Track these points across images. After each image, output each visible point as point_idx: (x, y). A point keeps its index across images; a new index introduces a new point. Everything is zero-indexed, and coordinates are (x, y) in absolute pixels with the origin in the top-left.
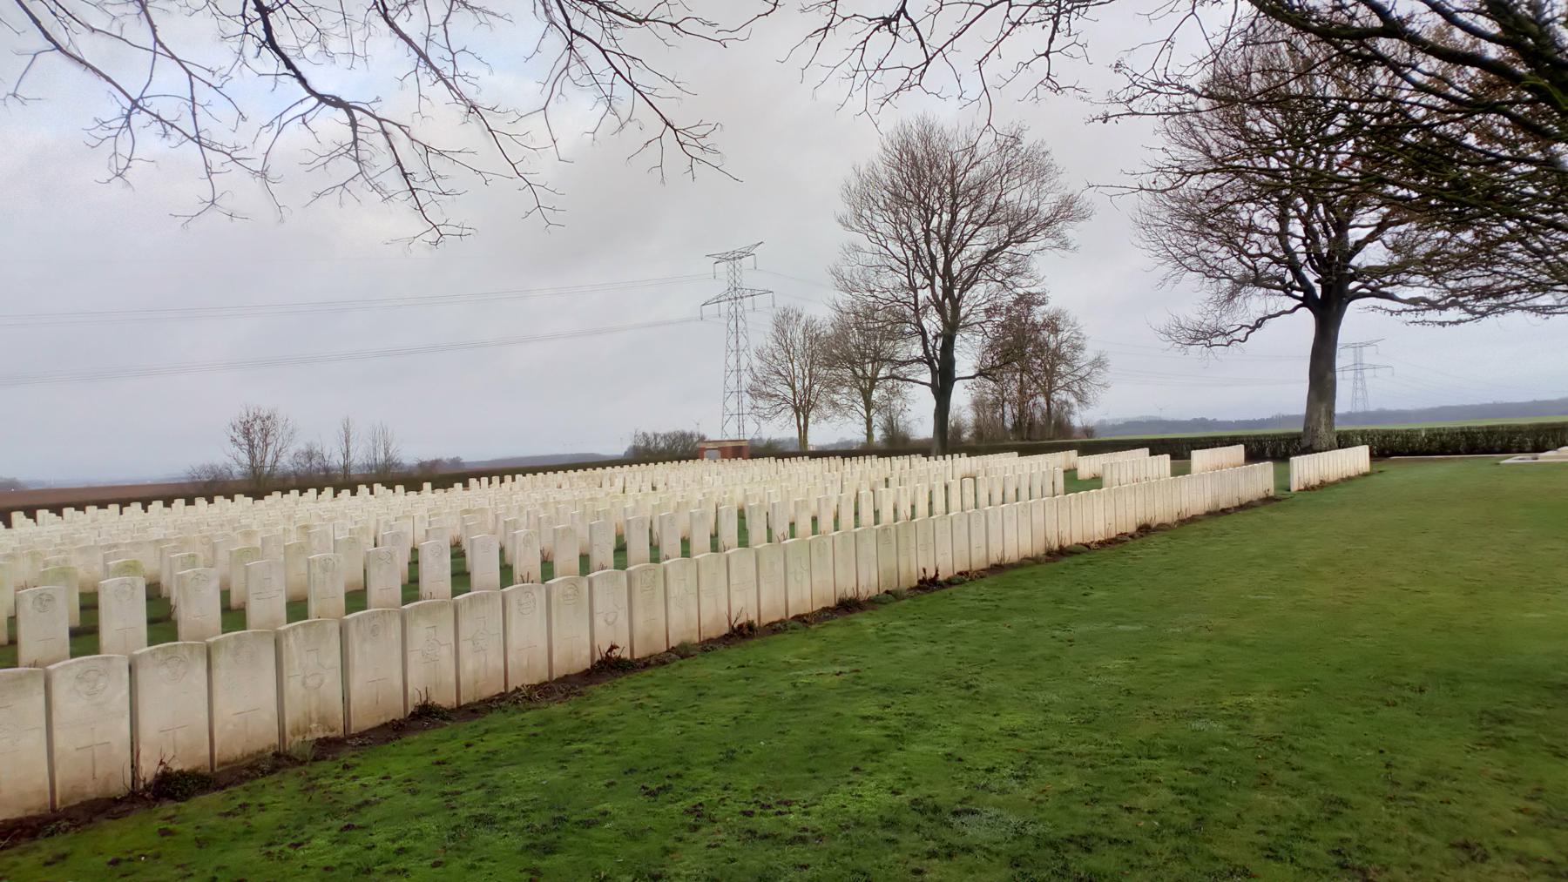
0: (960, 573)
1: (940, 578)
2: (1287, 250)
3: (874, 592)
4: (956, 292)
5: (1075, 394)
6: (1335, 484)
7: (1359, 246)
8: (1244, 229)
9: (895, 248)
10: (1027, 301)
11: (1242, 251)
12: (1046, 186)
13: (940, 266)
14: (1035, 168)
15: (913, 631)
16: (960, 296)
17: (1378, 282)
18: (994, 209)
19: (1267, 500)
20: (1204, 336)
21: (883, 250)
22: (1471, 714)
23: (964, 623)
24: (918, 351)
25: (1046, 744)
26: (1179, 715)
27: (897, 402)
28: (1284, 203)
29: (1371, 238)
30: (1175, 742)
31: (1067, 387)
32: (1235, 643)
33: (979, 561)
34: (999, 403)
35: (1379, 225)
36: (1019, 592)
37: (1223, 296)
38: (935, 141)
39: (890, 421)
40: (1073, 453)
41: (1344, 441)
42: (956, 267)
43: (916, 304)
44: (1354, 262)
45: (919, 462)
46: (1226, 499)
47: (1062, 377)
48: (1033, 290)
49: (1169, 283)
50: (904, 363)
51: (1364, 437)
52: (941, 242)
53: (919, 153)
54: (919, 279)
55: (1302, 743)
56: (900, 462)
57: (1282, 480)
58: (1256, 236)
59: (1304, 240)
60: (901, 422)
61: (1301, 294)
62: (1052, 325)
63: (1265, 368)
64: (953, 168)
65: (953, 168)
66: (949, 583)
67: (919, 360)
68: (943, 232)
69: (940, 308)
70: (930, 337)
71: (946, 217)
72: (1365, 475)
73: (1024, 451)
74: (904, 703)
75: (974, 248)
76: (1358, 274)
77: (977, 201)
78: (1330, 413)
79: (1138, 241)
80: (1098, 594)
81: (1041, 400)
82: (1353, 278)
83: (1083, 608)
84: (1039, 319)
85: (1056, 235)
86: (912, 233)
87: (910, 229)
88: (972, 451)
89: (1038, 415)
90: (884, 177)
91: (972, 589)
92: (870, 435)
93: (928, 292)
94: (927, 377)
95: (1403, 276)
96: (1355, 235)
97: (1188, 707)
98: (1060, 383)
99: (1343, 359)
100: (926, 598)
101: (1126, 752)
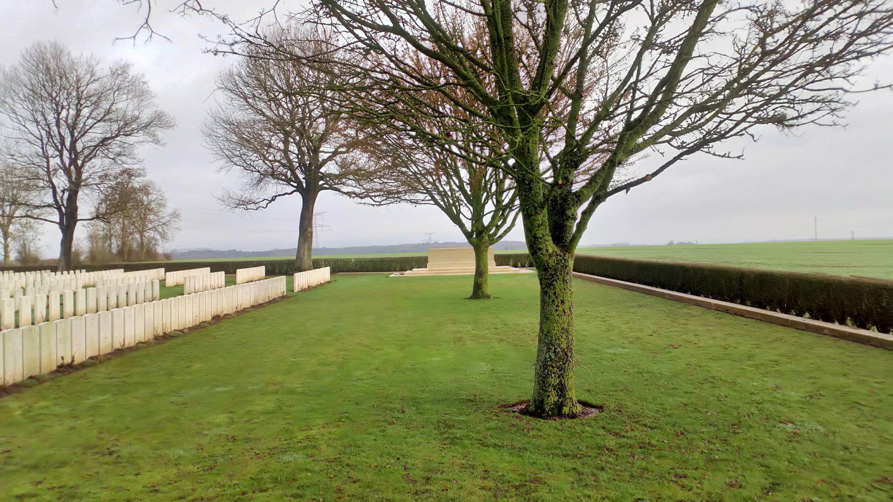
0: (92, 358)
1: (76, 363)
2: (289, 160)
3: (19, 379)
4: (79, 162)
5: (160, 233)
6: (315, 287)
7: (325, 162)
8: (266, 145)
9: (33, 127)
10: (129, 173)
11: (265, 159)
12: (144, 103)
13: (68, 143)
14: (139, 92)
15: (56, 410)
16: (83, 165)
17: (333, 182)
18: (108, 112)
19: (283, 298)
20: (243, 203)
21: (23, 128)
22: (432, 424)
23: (100, 398)
24: (51, 200)
25: (182, 494)
26: (273, 452)
27: (29, 234)
28: (287, 134)
29: (330, 159)
30: (275, 475)
31: (155, 229)
32: (292, 392)
33: (105, 347)
34: (108, 237)
35: (333, 152)
36: (140, 369)
37: (255, 182)
38: (64, 60)
39: (24, 246)
40: (163, 270)
41: (317, 265)
42: (79, 146)
43: (48, 168)
44: (323, 170)
45: (47, 275)
46: (262, 298)
47: (151, 222)
48: (135, 167)
49: (224, 171)
50: (37, 207)
51: (326, 263)
52: (68, 127)
53: (53, 65)
54: (51, 151)
55: (353, 460)
56: (31, 276)
57: (290, 288)
58: (272, 150)
59: (297, 155)
60: (32, 248)
61: (295, 185)
62: (145, 190)
63: (276, 223)
64: (78, 81)
65: (78, 81)
66: (83, 365)
67: (49, 206)
68: (70, 121)
69: (67, 172)
70: (58, 191)
71: (72, 112)
72: (328, 282)
73: (128, 268)
74: (56, 478)
75: (93, 135)
76: (324, 177)
77: (96, 104)
78: (310, 249)
79: (205, 144)
80: (197, 366)
81: (137, 236)
82: (322, 179)
83: (188, 377)
84: (137, 185)
85: (149, 134)
86: (46, 119)
87: (43, 115)
88: (90, 269)
89: (135, 245)
90: (25, 79)
91: (102, 369)
92: (6, 255)
93: (58, 160)
94: (57, 218)
95: (344, 180)
96: (323, 156)
97: (276, 444)
98: (150, 226)
99: (316, 220)
100: (65, 380)
101: (244, 489)
